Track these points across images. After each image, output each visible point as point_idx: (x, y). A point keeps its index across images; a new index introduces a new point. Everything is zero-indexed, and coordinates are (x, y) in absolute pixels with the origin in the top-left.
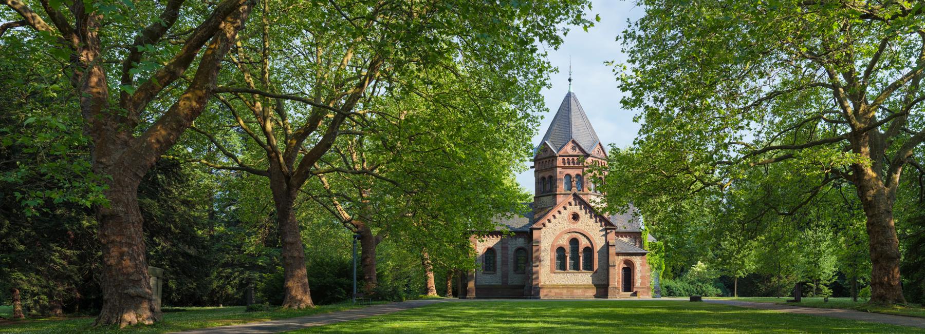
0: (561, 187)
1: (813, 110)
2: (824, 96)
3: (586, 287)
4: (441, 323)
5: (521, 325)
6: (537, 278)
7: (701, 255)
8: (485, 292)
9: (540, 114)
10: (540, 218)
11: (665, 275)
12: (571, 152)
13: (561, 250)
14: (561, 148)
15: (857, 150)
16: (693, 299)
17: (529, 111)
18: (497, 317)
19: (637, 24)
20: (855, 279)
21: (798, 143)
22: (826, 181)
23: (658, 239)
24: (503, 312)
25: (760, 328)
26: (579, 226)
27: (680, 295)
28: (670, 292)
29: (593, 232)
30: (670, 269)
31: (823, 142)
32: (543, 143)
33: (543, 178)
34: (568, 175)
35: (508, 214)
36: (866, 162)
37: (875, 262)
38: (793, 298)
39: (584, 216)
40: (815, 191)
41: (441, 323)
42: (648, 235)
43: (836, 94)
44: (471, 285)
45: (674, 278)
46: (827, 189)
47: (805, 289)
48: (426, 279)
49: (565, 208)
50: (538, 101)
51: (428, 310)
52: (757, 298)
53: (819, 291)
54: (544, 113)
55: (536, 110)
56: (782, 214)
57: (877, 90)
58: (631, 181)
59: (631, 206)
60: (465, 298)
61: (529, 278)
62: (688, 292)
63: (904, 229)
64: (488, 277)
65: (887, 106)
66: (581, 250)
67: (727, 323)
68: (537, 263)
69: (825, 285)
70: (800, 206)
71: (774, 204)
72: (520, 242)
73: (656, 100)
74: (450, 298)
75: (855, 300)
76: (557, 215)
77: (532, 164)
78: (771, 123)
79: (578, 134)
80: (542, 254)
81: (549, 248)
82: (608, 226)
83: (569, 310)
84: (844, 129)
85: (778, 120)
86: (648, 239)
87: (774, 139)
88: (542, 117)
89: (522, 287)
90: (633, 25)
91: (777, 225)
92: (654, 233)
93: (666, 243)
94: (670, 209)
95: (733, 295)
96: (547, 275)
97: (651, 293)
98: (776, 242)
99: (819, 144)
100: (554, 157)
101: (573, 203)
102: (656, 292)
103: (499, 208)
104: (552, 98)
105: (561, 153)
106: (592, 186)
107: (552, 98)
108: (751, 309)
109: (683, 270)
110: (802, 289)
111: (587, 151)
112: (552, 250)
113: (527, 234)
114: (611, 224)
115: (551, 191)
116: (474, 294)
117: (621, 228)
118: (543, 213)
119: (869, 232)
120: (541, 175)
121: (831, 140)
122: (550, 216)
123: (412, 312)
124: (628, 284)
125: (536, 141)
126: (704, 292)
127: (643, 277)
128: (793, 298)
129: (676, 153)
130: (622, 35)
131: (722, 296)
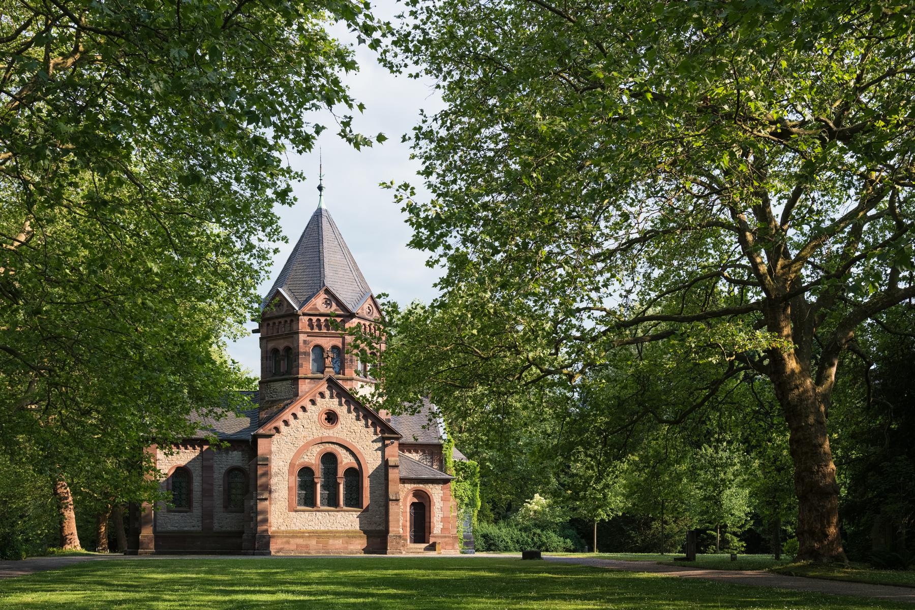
0: (307, 366)
1: (711, 260)
2: (727, 239)
3: (349, 536)
4: (107, 593)
5: (248, 597)
6: (265, 521)
7: (540, 483)
8: (172, 544)
9: (273, 245)
10: (270, 419)
11: (482, 515)
12: (323, 309)
13: (306, 473)
14: (306, 301)
15: (775, 328)
16: (527, 555)
17: (254, 240)
18: (206, 585)
19: (436, 119)
20: (776, 523)
21: (684, 314)
22: (732, 372)
23: (470, 457)
24: (210, 577)
25: (631, 599)
26: (337, 432)
27: (507, 549)
28: (490, 544)
29: (361, 443)
30: (488, 506)
31: (726, 312)
32: (275, 293)
33: (275, 351)
34: (319, 348)
35: (219, 411)
36: (788, 347)
37: (803, 498)
38: (684, 555)
39: (346, 417)
40: (715, 386)
41: (110, 595)
42: (454, 449)
43: (742, 241)
44: (147, 533)
45: (496, 521)
46: (732, 384)
47: (703, 540)
48: (61, 519)
49: (313, 402)
50: (269, 223)
51: (72, 573)
52: (629, 555)
53: (724, 545)
54: (280, 244)
55: (266, 239)
56: (666, 422)
57: (804, 235)
58: (425, 360)
59: (426, 401)
60: (136, 554)
61: (251, 519)
62: (519, 545)
63: (846, 450)
64: (177, 517)
65: (817, 261)
66: (341, 472)
67: (580, 592)
68: (265, 496)
69: (735, 534)
70: (693, 409)
71: (650, 400)
72: (236, 458)
73: (465, 240)
74: (103, 554)
75: (777, 558)
76: (300, 414)
77: (256, 326)
78: (647, 277)
79: (335, 277)
80: (274, 481)
81: (286, 470)
82: (386, 433)
83: (324, 573)
84: (754, 296)
85: (657, 273)
86: (454, 455)
87: (652, 303)
88: (276, 251)
89: (239, 534)
90: (430, 120)
91: (659, 437)
92: (460, 446)
93: (482, 463)
94: (489, 408)
95: (591, 550)
96: (285, 517)
97: (459, 546)
98: (658, 463)
99: (719, 314)
100: (294, 317)
101: (327, 394)
102: (466, 544)
103: (201, 399)
104: (292, 221)
105: (306, 309)
106: (360, 367)
107: (292, 221)
108: (619, 571)
109: (511, 508)
110: (698, 541)
111: (350, 307)
112: (290, 473)
113: (247, 445)
114: (392, 431)
115: (289, 372)
116: (152, 546)
117: (408, 438)
118: (275, 409)
119: (792, 453)
120: (271, 345)
121: (737, 310)
122: (287, 415)
123: (42, 577)
124: (421, 528)
125: (263, 290)
126: (544, 544)
127: (444, 520)
128: (684, 555)
129: (496, 326)
130: (412, 134)
131: (574, 551)
